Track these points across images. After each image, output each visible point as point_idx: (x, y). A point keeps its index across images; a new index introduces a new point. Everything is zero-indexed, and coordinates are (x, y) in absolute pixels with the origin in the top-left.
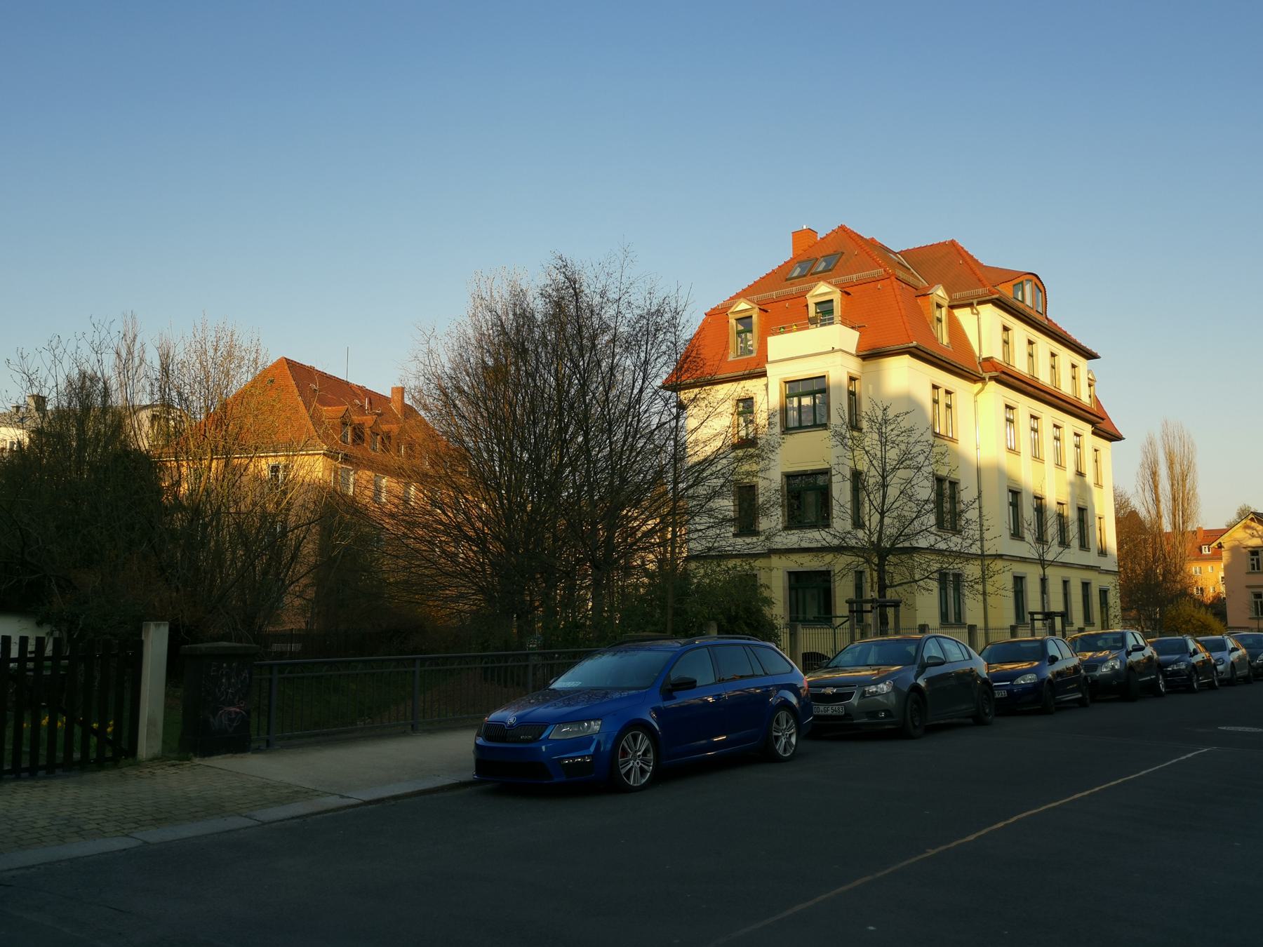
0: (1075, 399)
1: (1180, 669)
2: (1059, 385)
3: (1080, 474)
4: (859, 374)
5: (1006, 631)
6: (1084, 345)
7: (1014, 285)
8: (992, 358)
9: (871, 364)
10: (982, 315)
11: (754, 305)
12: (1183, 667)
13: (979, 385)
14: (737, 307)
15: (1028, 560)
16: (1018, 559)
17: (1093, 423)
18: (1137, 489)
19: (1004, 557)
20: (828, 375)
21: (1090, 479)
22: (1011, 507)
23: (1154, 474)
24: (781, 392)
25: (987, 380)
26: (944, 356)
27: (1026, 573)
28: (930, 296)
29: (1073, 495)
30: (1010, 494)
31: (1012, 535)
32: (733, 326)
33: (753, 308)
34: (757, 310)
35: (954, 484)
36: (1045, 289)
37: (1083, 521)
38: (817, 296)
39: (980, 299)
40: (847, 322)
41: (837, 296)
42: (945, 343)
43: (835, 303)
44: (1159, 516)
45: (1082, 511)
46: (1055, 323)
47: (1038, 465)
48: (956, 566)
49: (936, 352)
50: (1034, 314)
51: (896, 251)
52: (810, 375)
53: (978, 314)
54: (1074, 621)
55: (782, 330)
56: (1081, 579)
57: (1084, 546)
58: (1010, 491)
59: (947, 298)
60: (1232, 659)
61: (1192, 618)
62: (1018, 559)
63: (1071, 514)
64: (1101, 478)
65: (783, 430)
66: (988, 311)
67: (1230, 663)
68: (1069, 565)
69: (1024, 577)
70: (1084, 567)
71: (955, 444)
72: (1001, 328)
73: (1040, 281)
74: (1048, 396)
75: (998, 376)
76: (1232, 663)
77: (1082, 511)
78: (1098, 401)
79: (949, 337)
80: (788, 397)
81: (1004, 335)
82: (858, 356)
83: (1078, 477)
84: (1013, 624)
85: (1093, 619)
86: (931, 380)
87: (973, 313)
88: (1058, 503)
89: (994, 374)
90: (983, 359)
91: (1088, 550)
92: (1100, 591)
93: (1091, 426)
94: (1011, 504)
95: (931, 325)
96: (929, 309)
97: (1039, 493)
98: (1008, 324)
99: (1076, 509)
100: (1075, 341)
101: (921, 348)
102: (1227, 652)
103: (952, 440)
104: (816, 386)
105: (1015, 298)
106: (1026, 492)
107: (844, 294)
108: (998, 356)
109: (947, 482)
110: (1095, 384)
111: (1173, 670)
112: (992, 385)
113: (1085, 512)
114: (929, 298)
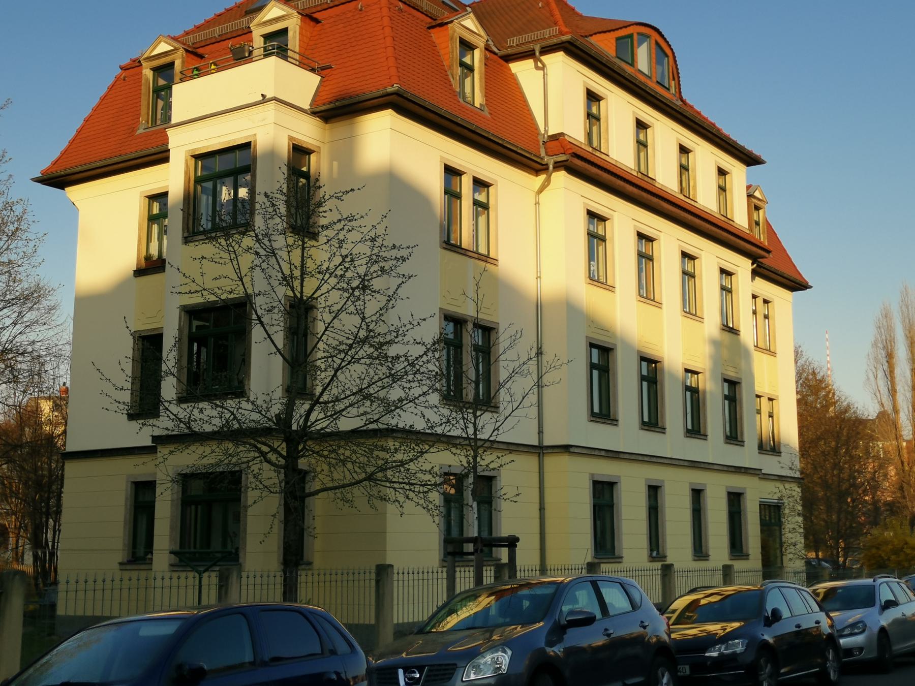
0: (723, 218)
1: (734, 654)
2: (695, 195)
3: (730, 330)
4: (317, 144)
6: (750, 149)
7: (618, 39)
8: (562, 134)
9: (340, 128)
10: (550, 69)
11: (177, 45)
12: (740, 649)
13: (543, 177)
14: (154, 49)
15: (622, 456)
16: (603, 453)
17: (754, 258)
18: (867, 376)
19: (572, 450)
20: (255, 141)
21: (747, 335)
22: (727, 402)
23: (890, 356)
24: (187, 173)
25: (551, 167)
27: (619, 477)
28: (450, 25)
29: (716, 359)
30: (726, 385)
32: (147, 80)
33: (176, 49)
34: (181, 52)
35: (487, 330)
36: (673, 53)
37: (735, 401)
38: (265, 23)
39: (545, 43)
40: (306, 63)
41: (294, 23)
42: (477, 104)
43: (290, 34)
44: (896, 411)
45: (733, 384)
46: (699, 110)
47: (650, 309)
48: (488, 460)
49: (461, 116)
50: (652, 85)
51: (467, 4)
52: (229, 142)
53: (543, 68)
54: (711, 552)
55: (196, 72)
56: (727, 487)
57: (734, 437)
58: (726, 380)
59: (482, 33)
60: (884, 623)
61: (905, 546)
62: (603, 453)
63: (710, 385)
65: (186, 235)
66: (558, 62)
67: (876, 630)
68: (702, 466)
69: (743, 494)
71: (496, 267)
72: (676, 149)
73: (665, 39)
74: (690, 217)
75: (567, 160)
76: (883, 630)
77: (733, 384)
78: (769, 224)
79: (486, 96)
80: (198, 181)
81: (721, 180)
82: (314, 113)
83: (727, 336)
84: (589, 559)
85: (747, 548)
86: (442, 157)
87: (537, 68)
88: (687, 371)
89: (562, 158)
90: (549, 137)
91: (741, 443)
92: (760, 505)
94: (726, 397)
95: (449, 73)
96: (448, 47)
97: (653, 351)
98: (688, 144)
99: (720, 381)
100: (735, 142)
101: (409, 96)
102: (876, 609)
103: (486, 258)
104: (239, 159)
105: (618, 58)
106: (627, 345)
107: (308, 20)
108: (576, 131)
109: (470, 326)
110: (766, 206)
111: (721, 655)
112: (561, 178)
114: (448, 28)
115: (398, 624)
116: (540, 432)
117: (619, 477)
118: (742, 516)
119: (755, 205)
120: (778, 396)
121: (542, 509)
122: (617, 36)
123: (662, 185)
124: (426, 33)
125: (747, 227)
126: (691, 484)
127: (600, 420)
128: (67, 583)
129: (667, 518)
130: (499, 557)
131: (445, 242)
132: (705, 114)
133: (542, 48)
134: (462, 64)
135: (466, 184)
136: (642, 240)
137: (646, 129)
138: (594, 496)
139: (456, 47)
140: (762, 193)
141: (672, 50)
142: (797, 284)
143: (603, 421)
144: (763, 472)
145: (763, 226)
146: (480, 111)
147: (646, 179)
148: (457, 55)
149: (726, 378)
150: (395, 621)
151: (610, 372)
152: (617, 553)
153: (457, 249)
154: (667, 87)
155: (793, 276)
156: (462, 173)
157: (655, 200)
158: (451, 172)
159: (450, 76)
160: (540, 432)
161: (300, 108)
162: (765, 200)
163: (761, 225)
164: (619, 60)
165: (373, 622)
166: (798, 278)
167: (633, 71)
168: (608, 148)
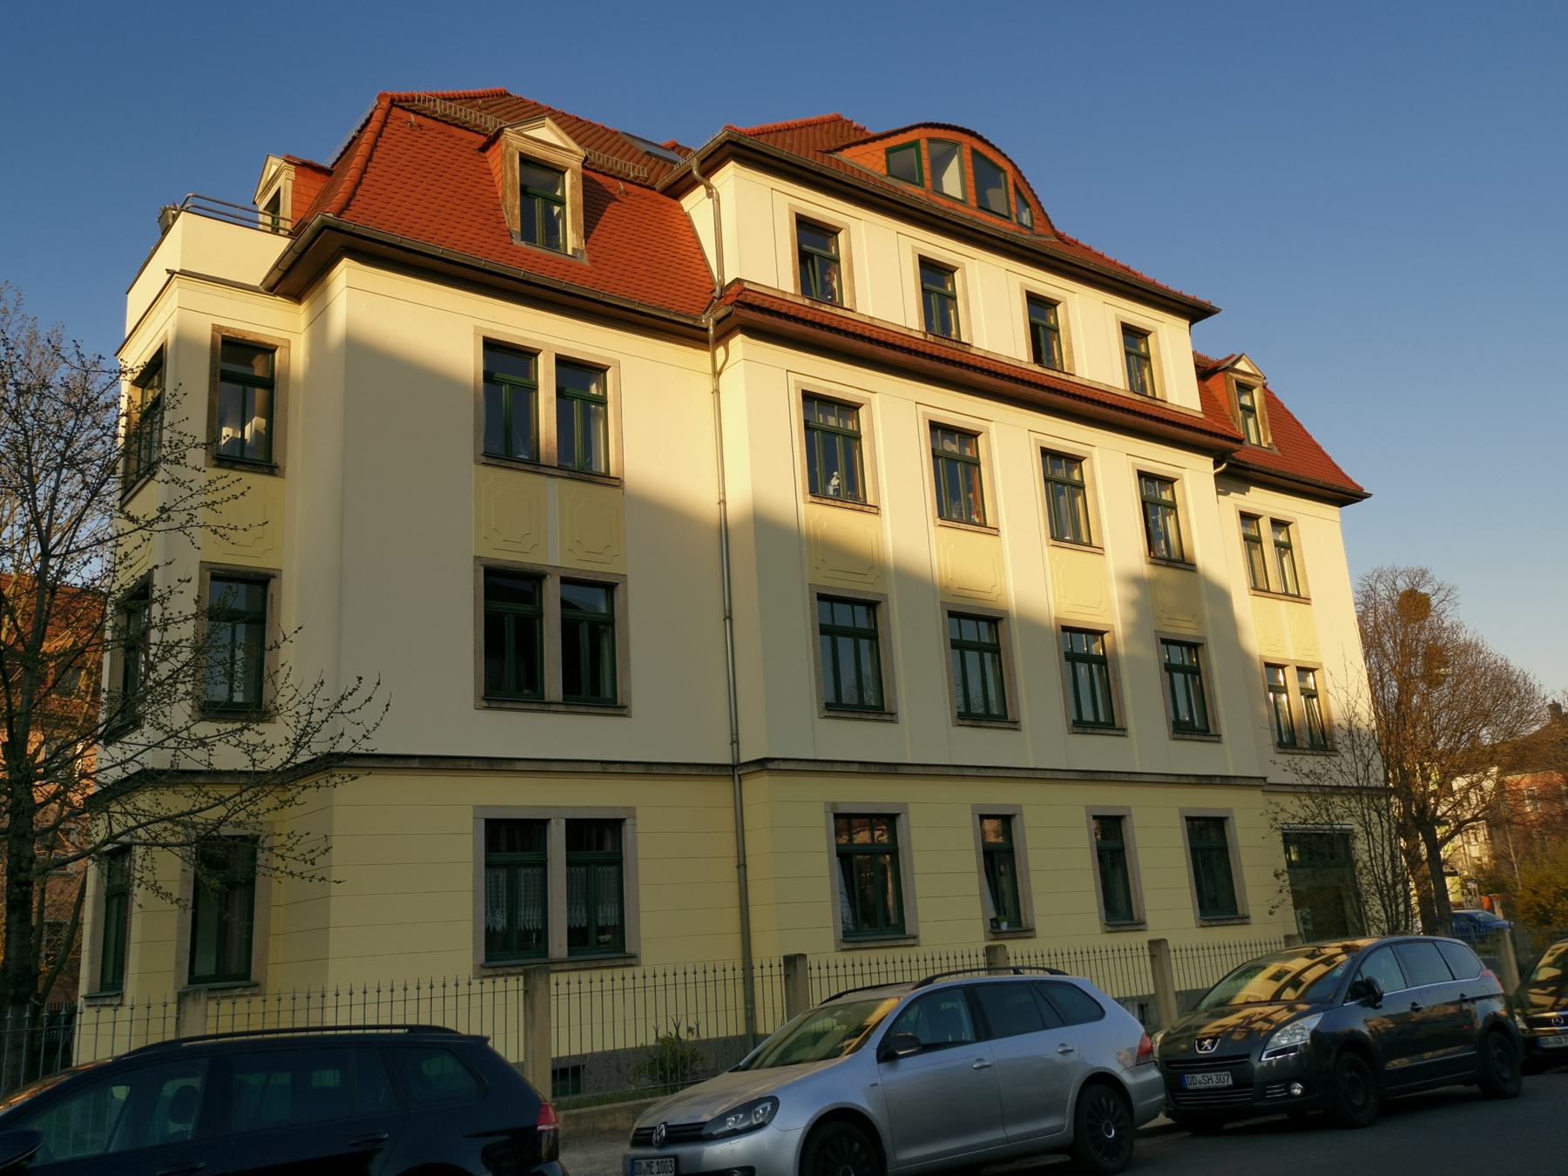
5: (171, 1023)
7: (889, 151)
16: (856, 768)
19: (771, 766)
26: (1274, 467)
31: (828, 706)
59: (574, 146)
62: (856, 768)
64: (1306, 582)
68: (1113, 777)
70: (1192, 780)
73: (992, 146)
83: (1170, 574)
93: (1209, 461)
105: (892, 176)
112: (739, 343)
113: (1001, 626)
115: (558, 1059)
116: (735, 741)
117: (1020, 806)
118: (1016, 858)
119: (1236, 382)
120: (1321, 664)
121: (742, 866)
122: (888, 146)
123: (1178, 406)
124: (478, 158)
125: (1199, 408)
126: (1181, 809)
127: (850, 715)
128: (762, 967)
129: (1032, 866)
130: (1246, 913)
131: (1252, 588)
132: (1109, 255)
133: (703, 162)
134: (1243, 407)
135: (1265, 526)
136: (1061, 460)
137: (1146, 336)
138: (1191, 838)
139: (512, 168)
140: (1251, 363)
141: (1011, 161)
142: (1350, 494)
143: (857, 715)
144: (1269, 780)
145: (1260, 413)
146: (1269, 451)
147: (1153, 402)
148: (514, 175)
149: (1165, 637)
150: (554, 1055)
151: (880, 639)
152: (1240, 912)
153: (601, 480)
154: (1006, 215)
155: (1337, 483)
156: (537, 352)
157: (1162, 426)
158: (1248, 518)
159: (1232, 421)
160: (735, 741)
161: (202, 275)
162: (1259, 374)
163: (1257, 411)
164: (895, 180)
165: (1152, 992)
166: (1352, 487)
167: (923, 193)
168: (854, 300)
